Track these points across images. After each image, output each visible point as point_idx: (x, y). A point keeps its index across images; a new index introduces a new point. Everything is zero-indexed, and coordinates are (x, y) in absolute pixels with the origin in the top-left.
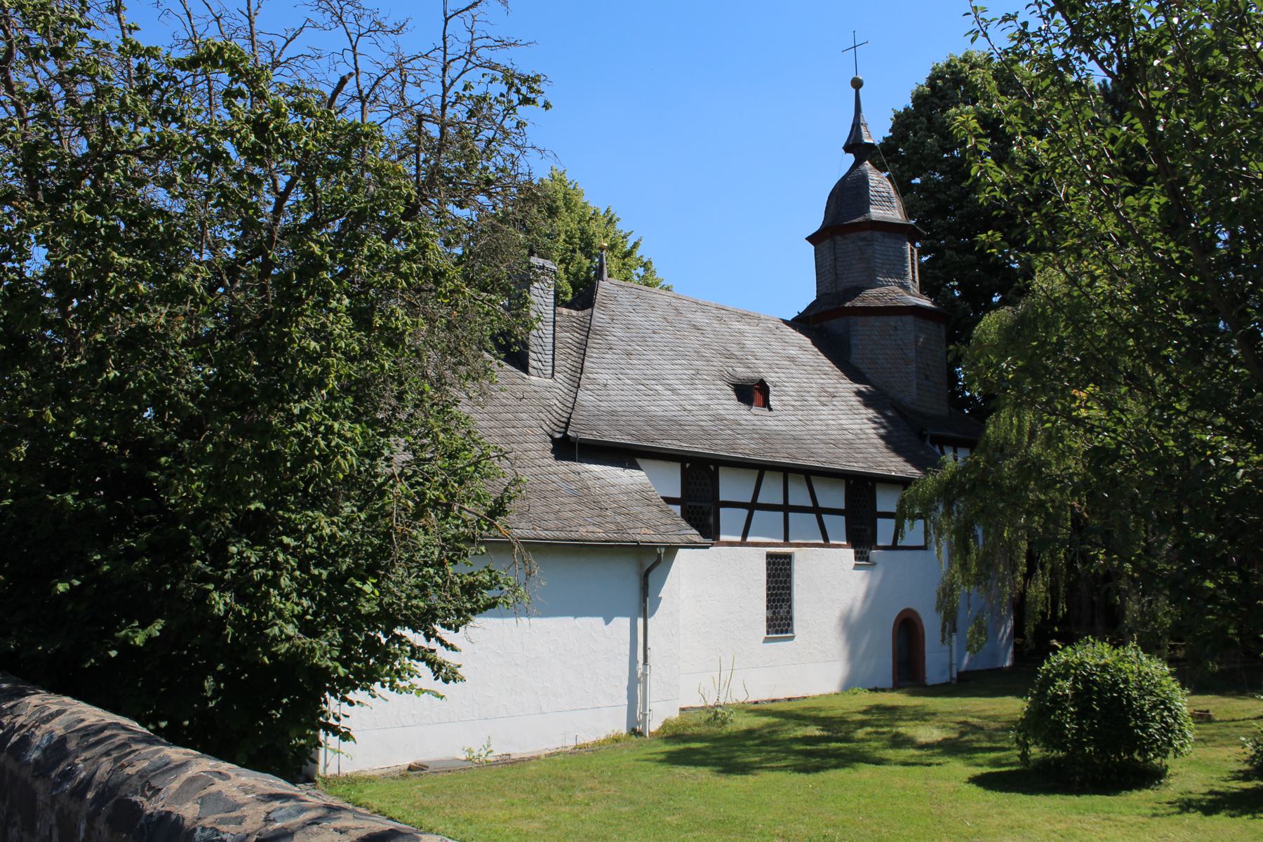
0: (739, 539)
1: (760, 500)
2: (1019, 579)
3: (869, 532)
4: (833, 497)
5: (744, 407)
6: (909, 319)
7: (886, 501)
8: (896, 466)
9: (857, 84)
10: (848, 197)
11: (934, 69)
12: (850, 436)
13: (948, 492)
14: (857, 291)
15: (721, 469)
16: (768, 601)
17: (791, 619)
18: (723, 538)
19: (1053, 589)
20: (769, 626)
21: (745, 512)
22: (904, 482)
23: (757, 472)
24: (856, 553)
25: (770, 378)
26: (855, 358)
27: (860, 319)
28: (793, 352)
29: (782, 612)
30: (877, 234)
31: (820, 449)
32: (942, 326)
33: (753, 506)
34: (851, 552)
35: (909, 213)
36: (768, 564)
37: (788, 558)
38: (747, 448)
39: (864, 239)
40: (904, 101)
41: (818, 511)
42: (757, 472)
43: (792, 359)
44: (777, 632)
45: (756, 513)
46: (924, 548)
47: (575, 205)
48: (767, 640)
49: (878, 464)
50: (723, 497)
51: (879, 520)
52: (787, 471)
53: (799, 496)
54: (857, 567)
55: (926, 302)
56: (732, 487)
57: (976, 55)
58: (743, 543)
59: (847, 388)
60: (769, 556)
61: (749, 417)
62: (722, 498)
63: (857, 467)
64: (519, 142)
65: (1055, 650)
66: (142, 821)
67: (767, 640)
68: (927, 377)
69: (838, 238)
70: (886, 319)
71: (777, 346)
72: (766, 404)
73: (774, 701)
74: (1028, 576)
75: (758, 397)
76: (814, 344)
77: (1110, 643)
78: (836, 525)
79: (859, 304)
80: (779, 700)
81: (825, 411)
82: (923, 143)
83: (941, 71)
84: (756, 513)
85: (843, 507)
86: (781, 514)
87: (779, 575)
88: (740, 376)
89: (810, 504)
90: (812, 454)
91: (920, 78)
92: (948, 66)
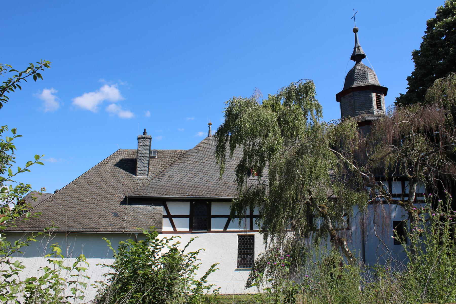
4: (185, 209)
9: (355, 31)
18: (212, 230)
30: (356, 93)
44: (244, 267)
48: (236, 270)
56: (215, 210)
58: (225, 231)
62: (213, 214)
67: (236, 270)
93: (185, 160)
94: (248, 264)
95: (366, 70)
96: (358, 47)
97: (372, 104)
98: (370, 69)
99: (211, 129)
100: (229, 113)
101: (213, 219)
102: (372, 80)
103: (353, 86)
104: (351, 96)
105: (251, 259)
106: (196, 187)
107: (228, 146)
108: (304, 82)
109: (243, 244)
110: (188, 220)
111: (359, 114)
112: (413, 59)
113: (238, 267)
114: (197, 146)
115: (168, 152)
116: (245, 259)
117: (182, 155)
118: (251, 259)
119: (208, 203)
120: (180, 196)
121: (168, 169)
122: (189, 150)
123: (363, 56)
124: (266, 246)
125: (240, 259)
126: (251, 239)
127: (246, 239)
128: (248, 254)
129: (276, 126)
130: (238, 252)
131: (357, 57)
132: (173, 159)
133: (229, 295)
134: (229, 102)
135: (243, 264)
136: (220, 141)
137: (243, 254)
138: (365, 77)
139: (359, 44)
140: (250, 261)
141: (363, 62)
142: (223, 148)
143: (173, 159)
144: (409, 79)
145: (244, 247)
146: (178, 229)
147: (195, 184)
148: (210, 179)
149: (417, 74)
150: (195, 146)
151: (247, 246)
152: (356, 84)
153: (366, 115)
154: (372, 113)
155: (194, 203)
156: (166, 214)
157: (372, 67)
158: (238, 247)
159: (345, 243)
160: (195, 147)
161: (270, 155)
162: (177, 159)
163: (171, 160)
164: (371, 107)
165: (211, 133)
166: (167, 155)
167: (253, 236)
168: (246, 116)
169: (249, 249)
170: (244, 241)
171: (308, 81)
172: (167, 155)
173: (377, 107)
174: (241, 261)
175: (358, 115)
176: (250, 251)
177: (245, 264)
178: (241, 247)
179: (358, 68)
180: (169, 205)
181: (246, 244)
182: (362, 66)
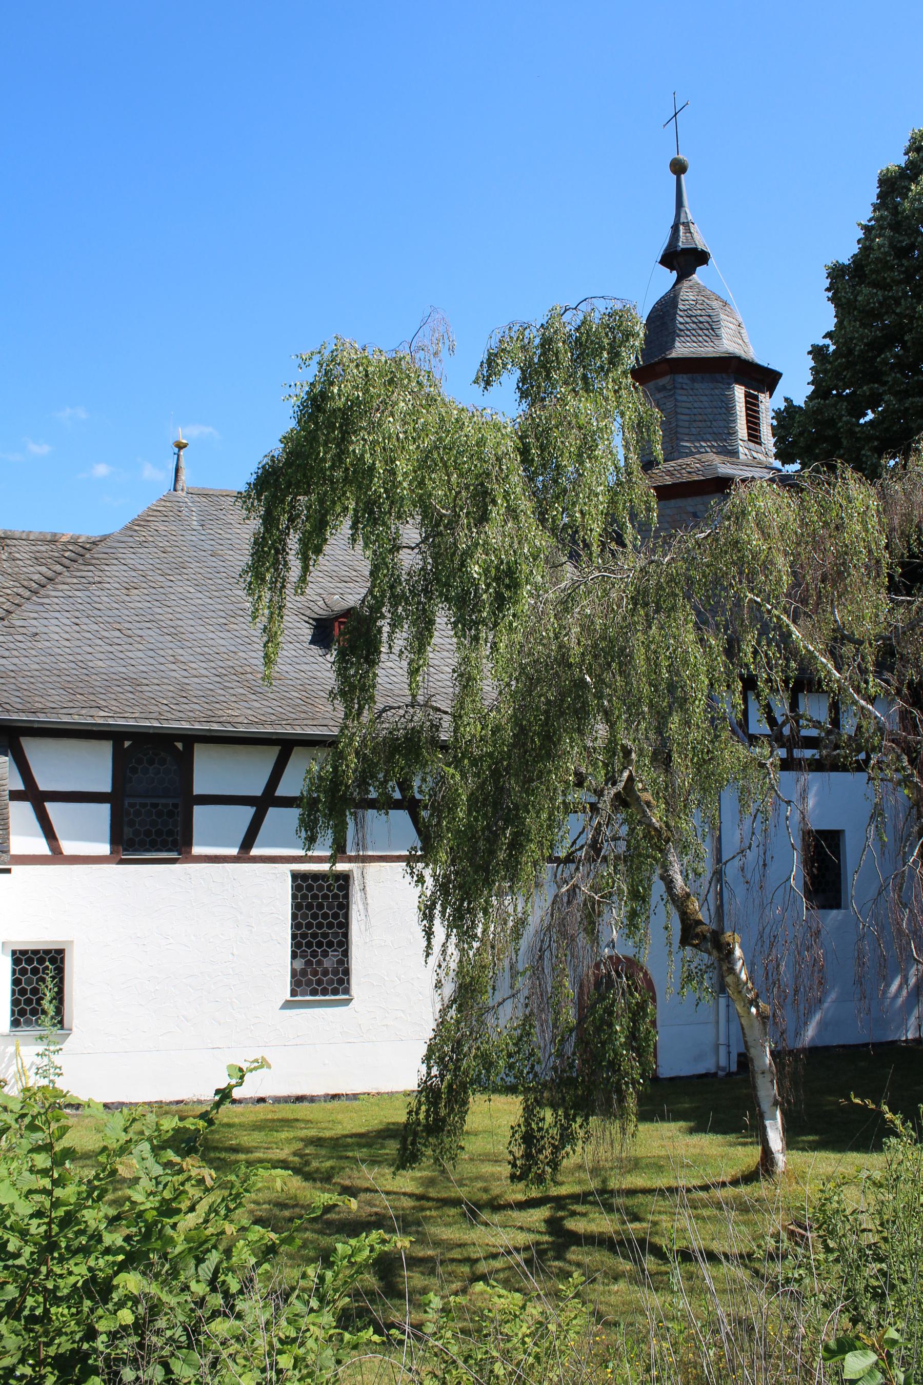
4: (94, 769)
9: (678, 168)
15: (199, 749)
17: (347, 972)
18: (197, 850)
30: (682, 379)
44: (314, 993)
48: (287, 1005)
50: (200, 788)
56: (210, 773)
58: (244, 855)
62: (198, 790)
64: (612, 428)
66: (631, 1103)
67: (287, 1005)
73: (300, 1099)
80: (312, 1099)
93: (91, 574)
94: (331, 982)
95: (715, 304)
96: (687, 225)
97: (734, 421)
98: (725, 304)
99: (183, 464)
100: (316, 404)
101: (199, 811)
102: (730, 342)
103: (674, 355)
104: (663, 388)
105: (340, 962)
106: (135, 683)
107: (293, 542)
108: (602, 307)
109: (310, 907)
110: (105, 809)
111: (691, 454)
112: (828, 290)
113: (293, 993)
114: (134, 522)
115: (26, 538)
116: (319, 963)
117: (80, 555)
118: (340, 962)
119: (179, 745)
120: (77, 719)
121: (27, 606)
122: (104, 539)
123: (701, 257)
124: (429, 946)
125: (299, 964)
126: (340, 888)
127: (320, 888)
128: (330, 944)
129: (515, 479)
130: (294, 937)
131: (683, 259)
132: (43, 569)
133: (262, 1100)
134: (317, 358)
135: (309, 982)
136: (269, 520)
137: (309, 945)
138: (711, 328)
139: (689, 213)
140: (335, 972)
141: (700, 275)
142: (277, 552)
143: (43, 569)
144: (817, 352)
145: (314, 916)
146: (68, 847)
147: (130, 672)
148: (185, 655)
149: (852, 339)
150: (126, 521)
151: (325, 916)
152: (682, 349)
153: (716, 459)
154: (734, 453)
155: (127, 744)
156: (21, 787)
157: (730, 297)
158: (294, 917)
159: (738, 952)
160: (128, 528)
161: (500, 602)
162: (59, 568)
163: (37, 572)
164: (731, 433)
165: (183, 476)
166: (23, 552)
167: (345, 879)
168: (393, 426)
169: (330, 926)
170: (315, 897)
171: (618, 306)
172: (23, 552)
173: (749, 435)
174: (303, 972)
175: (687, 455)
176: (336, 935)
177: (319, 982)
178: (304, 916)
179: (687, 295)
180: (33, 749)
181: (320, 907)
182: (700, 290)
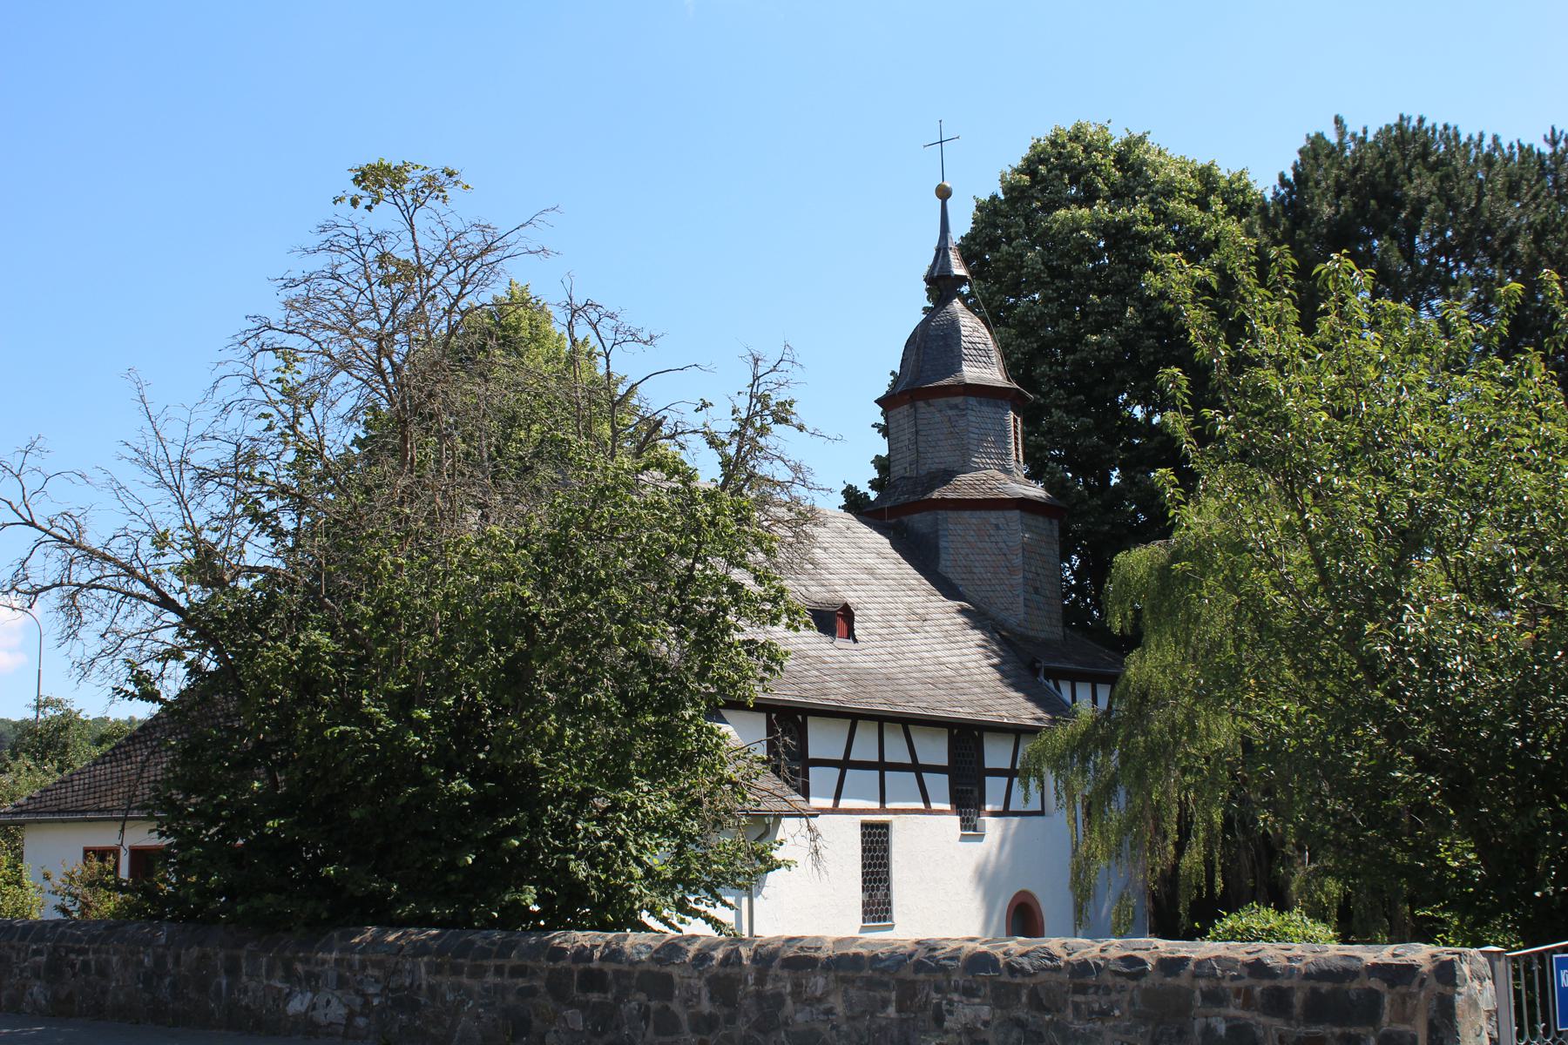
0: (876, 805)
1: (853, 757)
2: (1171, 847)
3: (976, 793)
4: (934, 750)
5: (826, 639)
6: (1015, 515)
7: (996, 754)
8: (1018, 709)
10: (931, 348)
11: (1033, 147)
12: (949, 673)
13: (1085, 746)
14: (946, 476)
15: (810, 719)
16: (864, 881)
17: (890, 903)
19: (1209, 864)
20: (865, 913)
21: (836, 772)
22: (1018, 732)
23: (849, 721)
24: (962, 820)
25: (851, 598)
26: (945, 564)
27: (951, 514)
28: (870, 560)
29: (880, 895)
30: (972, 401)
31: (918, 690)
32: (1055, 522)
33: (845, 764)
34: (958, 818)
35: (1011, 368)
36: (863, 835)
37: (885, 826)
38: (838, 694)
39: (956, 407)
40: (991, 188)
41: (917, 768)
42: (849, 721)
43: (870, 571)
45: (849, 772)
46: (1041, 813)
47: (546, 337)
49: (987, 709)
51: (988, 779)
52: (881, 719)
53: (897, 751)
54: (963, 838)
55: (1036, 491)
56: (823, 741)
57: (1092, 130)
58: (835, 810)
59: (944, 611)
60: (865, 825)
61: (832, 653)
63: (963, 712)
65: (1220, 917)
68: (1036, 591)
69: (921, 404)
70: (983, 514)
71: (851, 554)
72: (850, 634)
74: (1180, 848)
75: (841, 625)
76: (894, 546)
77: (1276, 908)
78: (939, 784)
79: (950, 496)
81: (917, 639)
82: (1021, 256)
83: (1044, 151)
84: (849, 772)
85: (945, 763)
86: (877, 773)
87: (876, 842)
88: (817, 598)
89: (908, 760)
90: (911, 699)
91: (1016, 155)
92: (1053, 143)
